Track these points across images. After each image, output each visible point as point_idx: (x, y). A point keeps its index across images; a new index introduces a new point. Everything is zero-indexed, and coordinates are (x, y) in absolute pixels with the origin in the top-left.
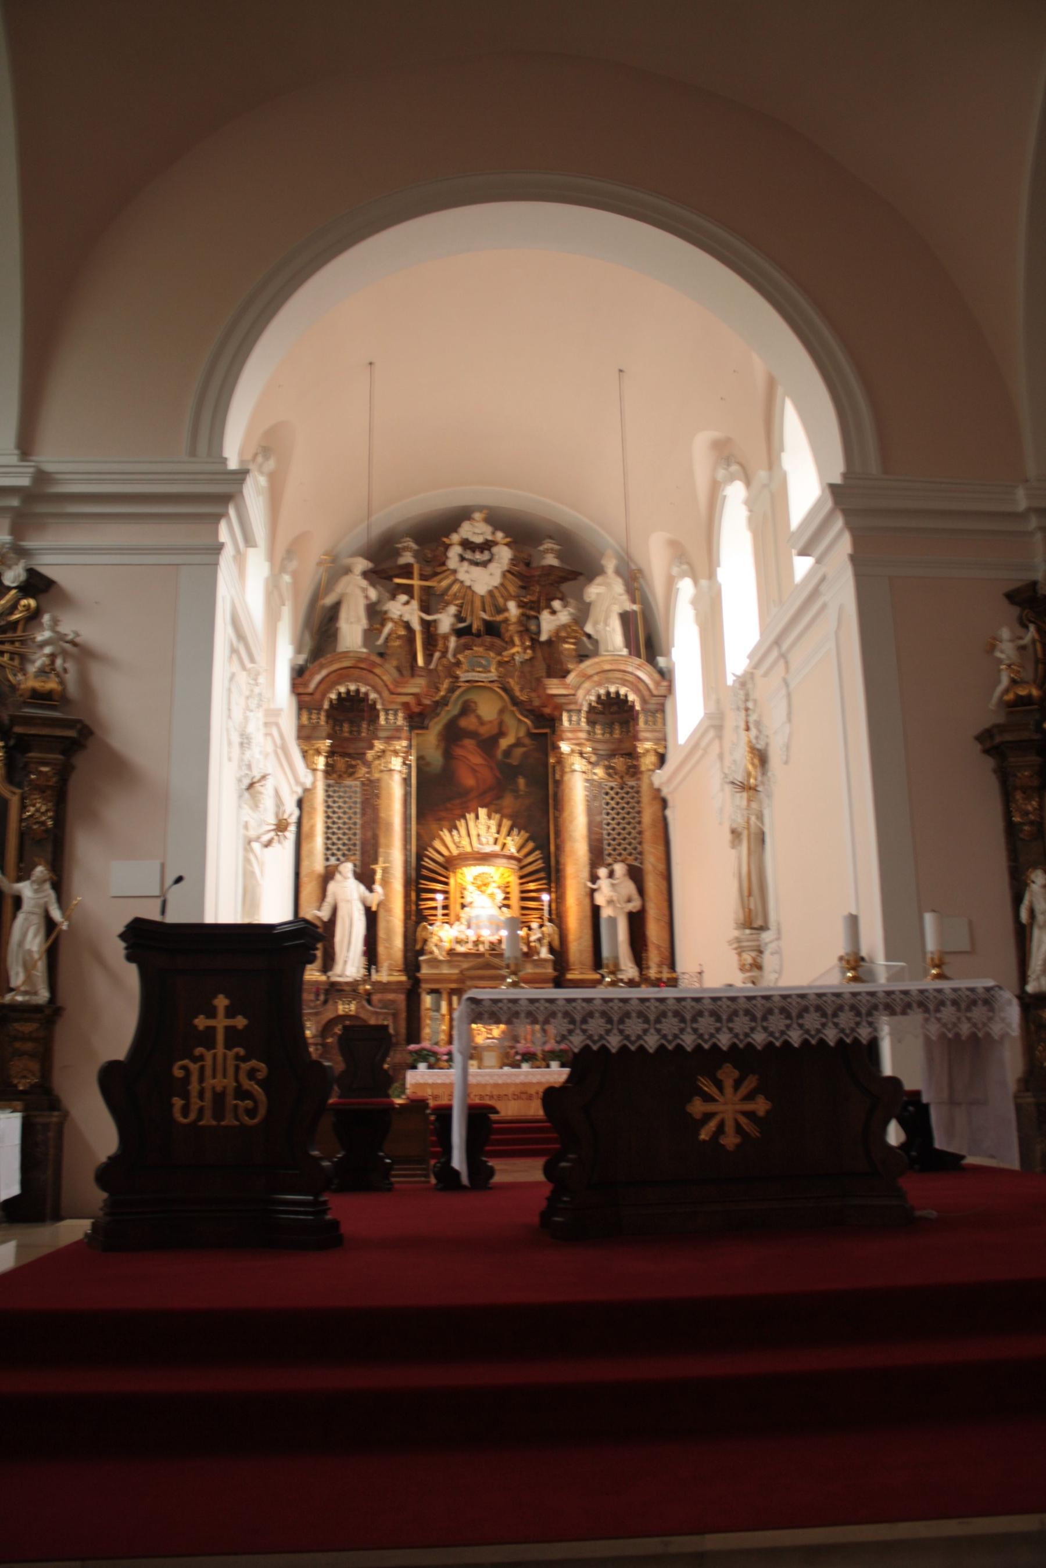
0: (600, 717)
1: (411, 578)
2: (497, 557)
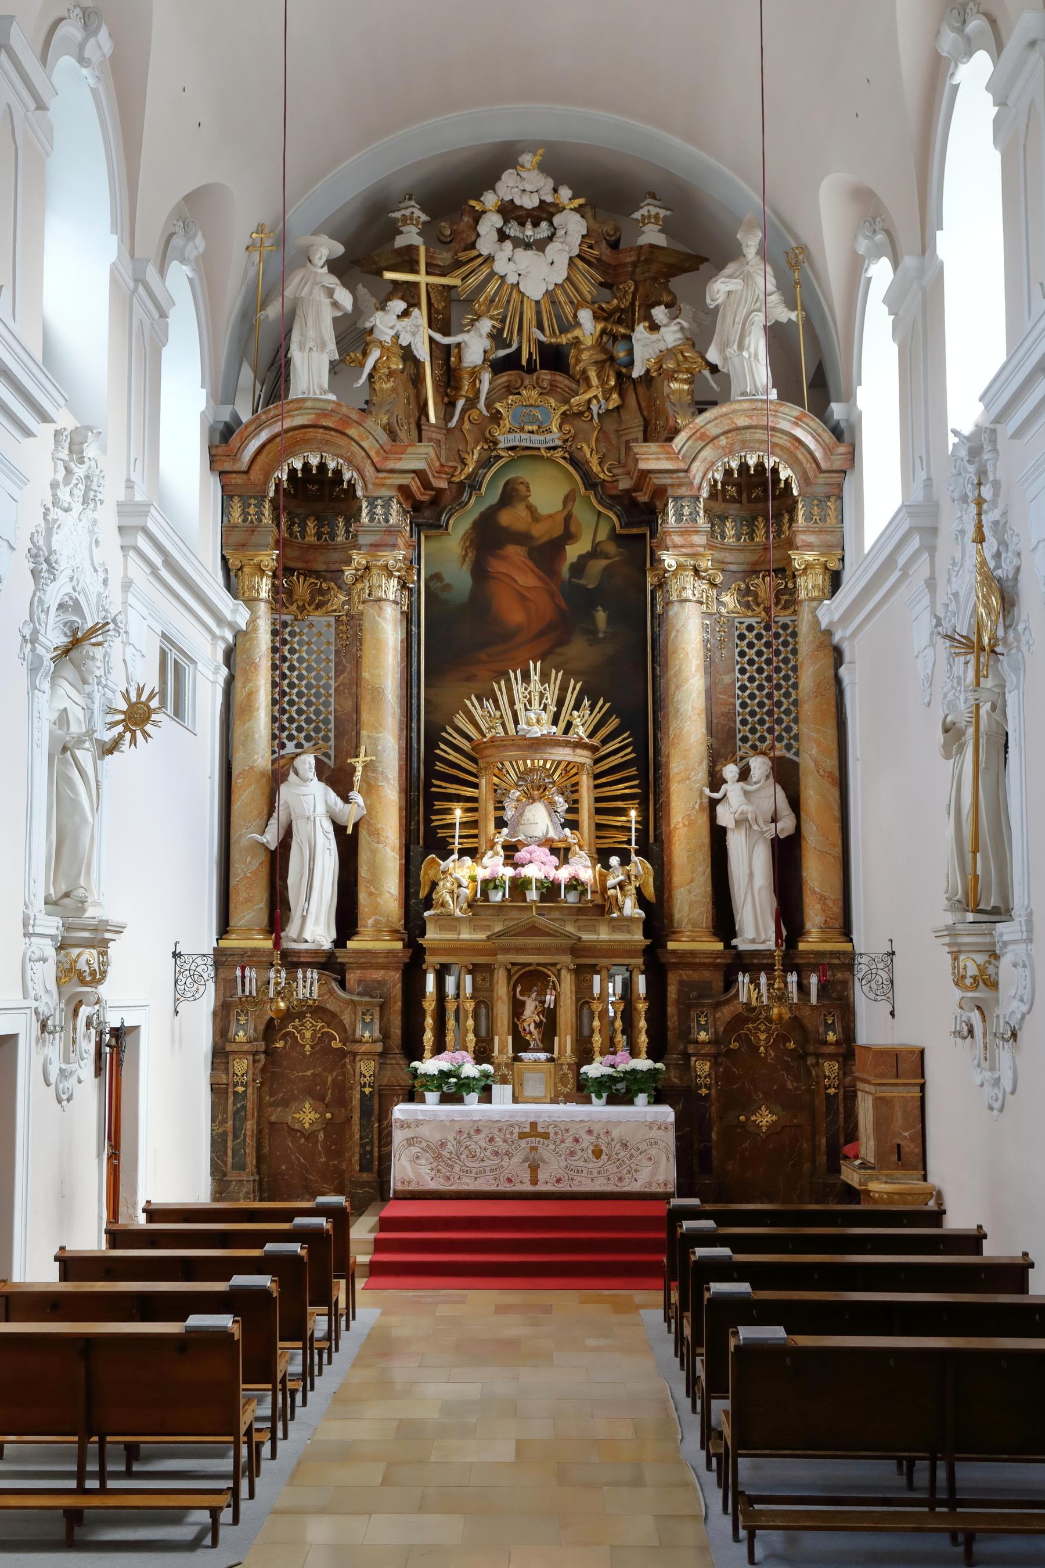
0: (733, 509)
1: (416, 272)
2: (560, 233)
